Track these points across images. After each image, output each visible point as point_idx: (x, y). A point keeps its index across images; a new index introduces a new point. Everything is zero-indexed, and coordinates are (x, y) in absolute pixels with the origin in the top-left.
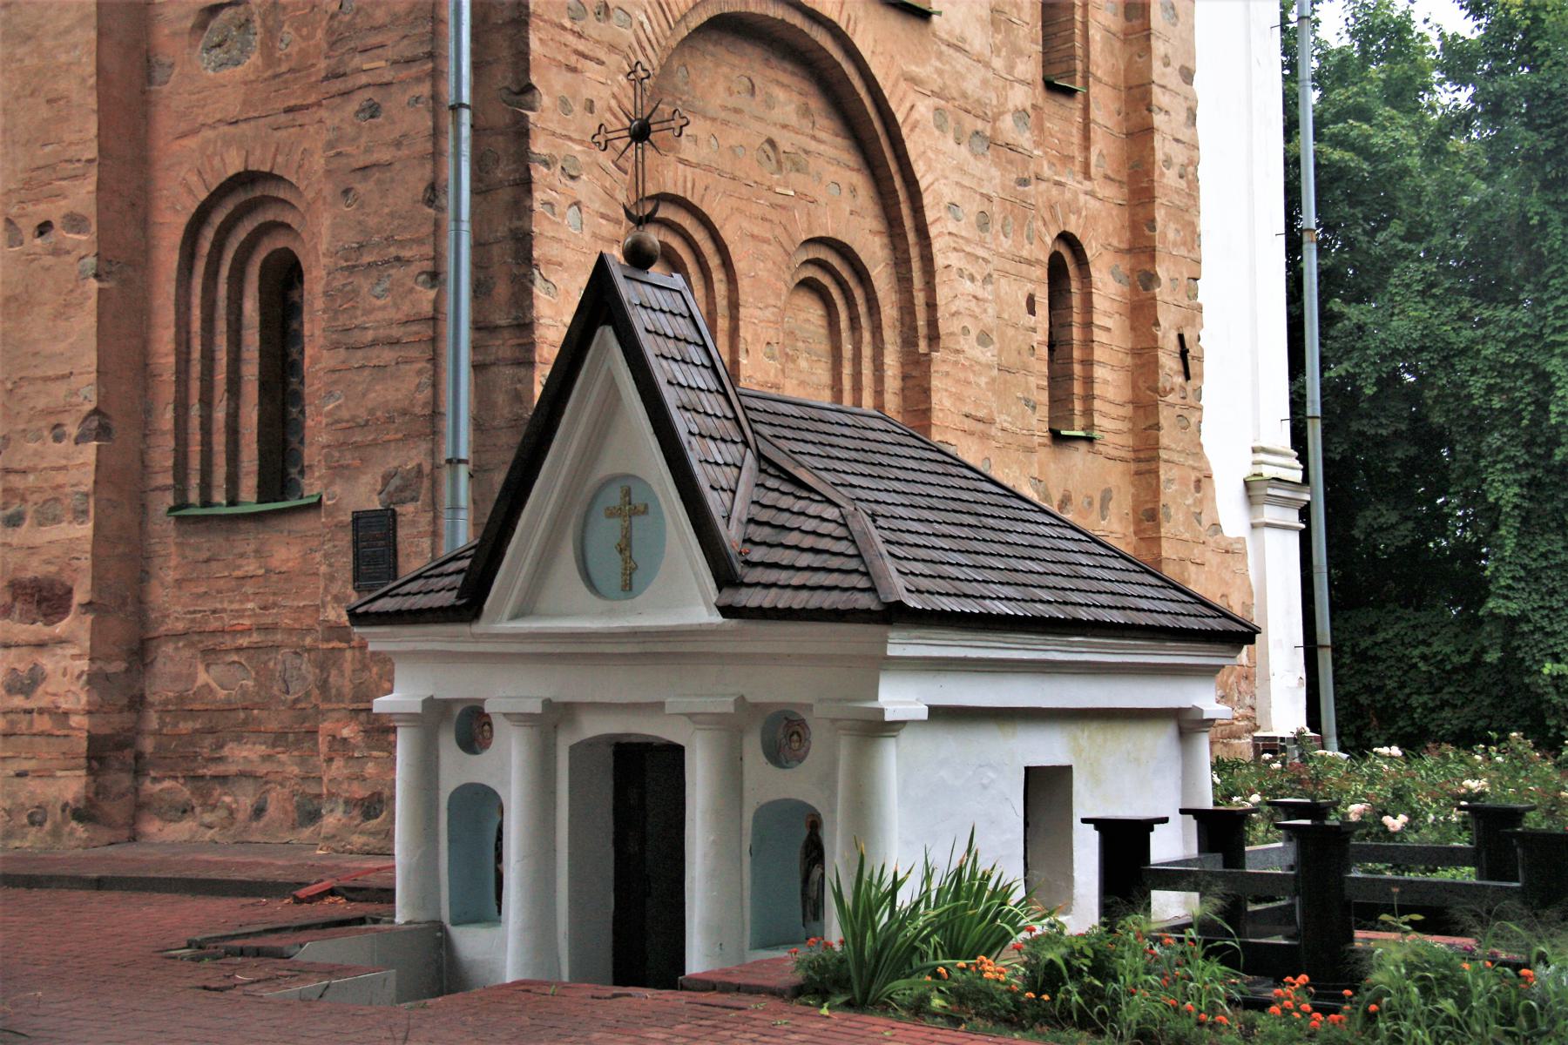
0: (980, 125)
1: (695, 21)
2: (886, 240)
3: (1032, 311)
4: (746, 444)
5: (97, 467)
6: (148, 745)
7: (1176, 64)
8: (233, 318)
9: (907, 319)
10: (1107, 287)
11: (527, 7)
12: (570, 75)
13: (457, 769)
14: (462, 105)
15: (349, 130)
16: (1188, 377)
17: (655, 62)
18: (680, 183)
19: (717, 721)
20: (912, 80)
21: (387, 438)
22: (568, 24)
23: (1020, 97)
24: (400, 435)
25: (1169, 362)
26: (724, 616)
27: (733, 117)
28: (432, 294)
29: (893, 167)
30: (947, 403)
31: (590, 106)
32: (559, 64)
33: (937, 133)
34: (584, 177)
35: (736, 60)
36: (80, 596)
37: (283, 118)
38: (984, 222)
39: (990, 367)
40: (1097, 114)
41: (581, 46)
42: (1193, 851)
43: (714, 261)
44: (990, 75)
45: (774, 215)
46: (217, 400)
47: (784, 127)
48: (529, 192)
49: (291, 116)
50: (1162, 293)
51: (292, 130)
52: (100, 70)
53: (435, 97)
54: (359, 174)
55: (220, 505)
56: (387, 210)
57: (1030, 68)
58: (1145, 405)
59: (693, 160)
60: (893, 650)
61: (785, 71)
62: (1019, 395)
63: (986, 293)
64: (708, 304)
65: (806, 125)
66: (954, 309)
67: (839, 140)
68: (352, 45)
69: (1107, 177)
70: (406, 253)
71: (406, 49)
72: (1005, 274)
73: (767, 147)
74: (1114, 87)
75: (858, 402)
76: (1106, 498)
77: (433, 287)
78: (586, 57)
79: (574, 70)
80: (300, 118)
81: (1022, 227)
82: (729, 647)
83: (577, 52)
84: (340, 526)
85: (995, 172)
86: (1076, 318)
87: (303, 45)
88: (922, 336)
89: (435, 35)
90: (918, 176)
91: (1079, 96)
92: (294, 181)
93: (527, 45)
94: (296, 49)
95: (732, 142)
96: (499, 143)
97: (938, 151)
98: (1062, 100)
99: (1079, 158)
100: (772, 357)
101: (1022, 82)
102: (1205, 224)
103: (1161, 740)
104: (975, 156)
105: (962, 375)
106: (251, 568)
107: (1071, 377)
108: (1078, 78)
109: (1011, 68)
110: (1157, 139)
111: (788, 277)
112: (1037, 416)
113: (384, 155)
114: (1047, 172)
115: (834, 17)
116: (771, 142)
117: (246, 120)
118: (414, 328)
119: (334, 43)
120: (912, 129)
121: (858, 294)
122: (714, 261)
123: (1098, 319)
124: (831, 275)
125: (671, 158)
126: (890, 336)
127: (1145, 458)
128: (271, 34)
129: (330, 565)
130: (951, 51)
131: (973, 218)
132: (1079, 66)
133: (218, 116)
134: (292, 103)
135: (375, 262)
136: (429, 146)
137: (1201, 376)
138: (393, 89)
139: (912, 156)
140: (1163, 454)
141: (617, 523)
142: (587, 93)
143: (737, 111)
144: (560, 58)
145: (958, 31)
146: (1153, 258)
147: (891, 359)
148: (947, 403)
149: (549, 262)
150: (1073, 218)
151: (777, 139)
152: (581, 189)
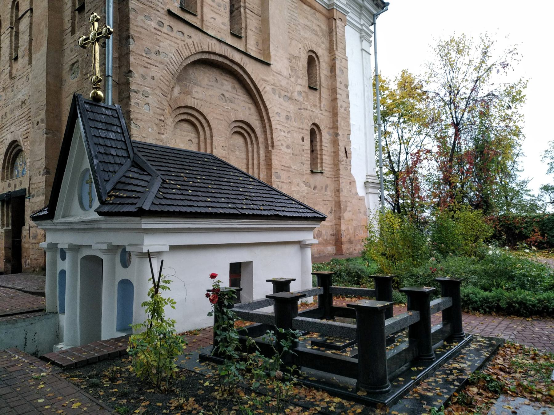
0: (286, 94)
1: (192, 59)
2: (260, 122)
4: (129, 157)
7: (343, 84)
10: (326, 136)
12: (145, 69)
14: (109, 76)
18: (193, 103)
20: (265, 81)
22: (145, 55)
23: (299, 88)
25: (342, 154)
27: (210, 87)
29: (260, 103)
30: (277, 162)
31: (153, 78)
32: (141, 66)
33: (273, 95)
34: (150, 97)
35: (211, 73)
38: (288, 118)
39: (290, 154)
40: (322, 95)
41: (149, 61)
42: (273, 293)
43: (205, 125)
44: (290, 82)
45: (223, 113)
48: (130, 100)
57: (304, 81)
58: (336, 165)
59: (197, 98)
60: (144, 226)
63: (289, 135)
65: (234, 91)
66: (278, 139)
67: (245, 96)
69: (326, 110)
72: (296, 131)
73: (222, 96)
74: (328, 89)
75: (206, 151)
76: (326, 187)
78: (151, 64)
82: (104, 226)
83: (147, 63)
86: (318, 144)
88: (270, 145)
91: (243, 39)
95: (210, 94)
97: (273, 99)
98: (314, 91)
99: (318, 105)
100: (224, 150)
101: (300, 85)
102: (352, 122)
103: (293, 250)
109: (296, 81)
111: (230, 130)
114: (309, 108)
115: (239, 62)
120: (265, 92)
121: (252, 135)
122: (205, 125)
123: (324, 144)
124: (243, 130)
125: (189, 96)
126: (262, 146)
127: (337, 177)
131: (284, 117)
132: (318, 83)
139: (265, 100)
140: (341, 176)
141: (88, 185)
142: (152, 74)
143: (211, 86)
144: (141, 64)
145: (279, 70)
147: (262, 152)
148: (277, 162)
149: (137, 119)
151: (225, 94)
152: (150, 100)
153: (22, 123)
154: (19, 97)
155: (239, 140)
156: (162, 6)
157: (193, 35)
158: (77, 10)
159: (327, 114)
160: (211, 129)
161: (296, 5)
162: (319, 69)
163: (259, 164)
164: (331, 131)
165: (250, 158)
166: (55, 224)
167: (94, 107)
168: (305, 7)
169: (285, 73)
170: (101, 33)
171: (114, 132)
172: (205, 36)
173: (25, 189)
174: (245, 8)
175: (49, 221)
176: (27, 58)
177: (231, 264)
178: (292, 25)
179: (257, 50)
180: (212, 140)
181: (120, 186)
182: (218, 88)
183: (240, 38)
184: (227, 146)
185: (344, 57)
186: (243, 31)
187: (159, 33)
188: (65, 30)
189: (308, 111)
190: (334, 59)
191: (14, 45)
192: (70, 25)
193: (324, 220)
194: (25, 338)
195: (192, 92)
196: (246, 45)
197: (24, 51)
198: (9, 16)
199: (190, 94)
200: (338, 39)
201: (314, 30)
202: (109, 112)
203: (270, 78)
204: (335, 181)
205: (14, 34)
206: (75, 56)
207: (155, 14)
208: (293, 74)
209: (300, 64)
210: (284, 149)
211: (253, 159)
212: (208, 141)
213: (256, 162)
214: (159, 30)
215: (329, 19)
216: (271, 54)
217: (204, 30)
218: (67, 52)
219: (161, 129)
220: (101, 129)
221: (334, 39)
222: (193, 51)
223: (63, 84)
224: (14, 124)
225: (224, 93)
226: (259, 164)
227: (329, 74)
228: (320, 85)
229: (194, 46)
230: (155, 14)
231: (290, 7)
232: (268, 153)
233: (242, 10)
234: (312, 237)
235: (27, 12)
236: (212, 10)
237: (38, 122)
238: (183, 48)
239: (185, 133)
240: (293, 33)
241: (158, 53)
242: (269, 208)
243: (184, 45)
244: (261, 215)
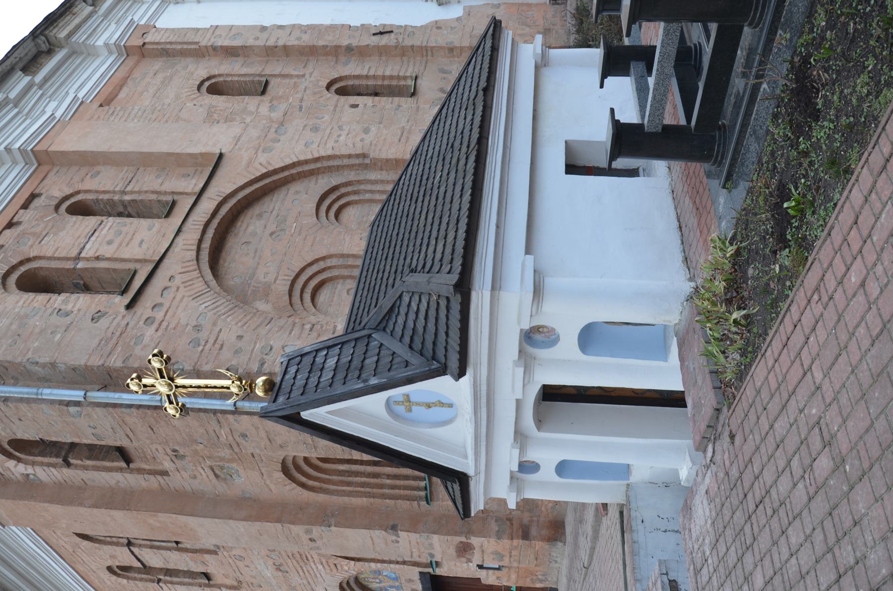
0: (273, 130)
1: (209, 276)
2: (320, 177)
3: (356, 106)
4: (369, 336)
5: (409, 531)
6: (539, 38)
7: (258, 34)
10: (352, 68)
12: (224, 348)
13: (547, 472)
16: (392, 32)
18: (284, 282)
19: (528, 370)
20: (249, 163)
22: (201, 348)
23: (264, 110)
25: (384, 40)
26: (464, 374)
29: (286, 173)
31: (240, 337)
32: (218, 354)
34: (271, 343)
36: (463, 539)
38: (315, 129)
40: (277, 72)
41: (211, 341)
47: (265, 227)
50: (355, 43)
52: (244, 520)
57: (251, 102)
58: (403, 52)
63: (346, 128)
65: (265, 215)
67: (276, 196)
69: (304, 67)
71: (214, 423)
73: (274, 236)
74: (267, 62)
76: (443, 71)
79: (222, 345)
83: (214, 345)
91: (176, 197)
98: (270, 88)
99: (296, 80)
101: (258, 108)
102: (327, 22)
103: (550, 79)
108: (261, 79)
109: (251, 113)
110: (289, 43)
111: (332, 227)
112: (403, 104)
113: (263, 434)
114: (299, 95)
115: (216, 203)
116: (272, 234)
120: (270, 164)
121: (343, 190)
123: (365, 73)
124: (332, 204)
125: (273, 287)
127: (425, 52)
128: (222, 459)
131: (313, 134)
132: (257, 79)
137: (392, 25)
140: (424, 44)
141: (414, 408)
142: (233, 338)
143: (256, 252)
146: (340, 47)
150: (320, 83)
153: (311, 572)
154: (269, 575)
156: (120, 317)
157: (169, 274)
158: (128, 465)
159: (310, 66)
160: (330, 256)
161: (119, 108)
162: (232, 75)
164: (342, 59)
166: (477, 473)
167: (282, 391)
168: (122, 95)
170: (160, 370)
171: (326, 360)
172: (169, 253)
173: (420, 573)
174: (124, 192)
175: (472, 484)
176: (207, 557)
177: (567, 173)
178: (154, 116)
181: (417, 345)
182: (260, 241)
183: (174, 203)
185: (211, 31)
186: (164, 198)
187: (165, 324)
188: (162, 489)
189: (305, 98)
190: (215, 48)
191: (187, 580)
192: (152, 477)
193: (500, 22)
194: (665, 531)
195: (266, 283)
197: (196, 562)
198: (140, 584)
200: (179, 40)
201: (162, 83)
202: (292, 370)
204: (432, 56)
205: (168, 578)
206: (202, 471)
207: (133, 329)
208: (238, 118)
210: (368, 138)
214: (160, 324)
215: (143, 56)
216: (204, 151)
217: (158, 258)
218: (196, 485)
219: (327, 330)
220: (319, 378)
221: (179, 47)
222: (196, 274)
223: (247, 495)
224: (314, 586)
225: (268, 232)
227: (240, 60)
228: (260, 75)
230: (133, 329)
231: (124, 118)
232: (375, 164)
233: (127, 198)
234: (530, 47)
235: (133, 553)
236: (128, 244)
237: (311, 540)
239: (335, 299)
240: (167, 116)
241: (198, 328)
242: (471, 107)
243: (185, 287)
244: (483, 116)
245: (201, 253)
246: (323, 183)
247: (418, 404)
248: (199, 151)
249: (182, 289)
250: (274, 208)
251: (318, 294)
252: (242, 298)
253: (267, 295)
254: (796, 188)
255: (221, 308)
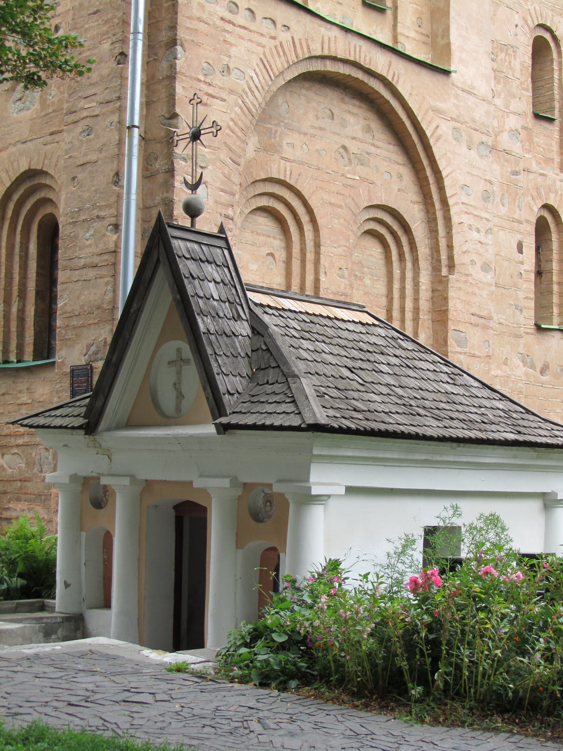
0: (484, 138)
1: (289, 76)
2: (422, 207)
3: (520, 251)
8: (23, 254)
9: (435, 254)
11: (175, 69)
15: (77, 143)
17: (260, 100)
18: (282, 172)
20: (437, 111)
21: (90, 322)
22: (202, 78)
23: (512, 122)
24: (96, 321)
28: (115, 237)
29: (425, 162)
33: (454, 142)
37: (49, 138)
38: (487, 196)
39: (490, 285)
41: (210, 90)
43: (305, 218)
46: (13, 302)
47: (353, 138)
48: (173, 176)
49: (53, 137)
51: (53, 145)
53: (121, 122)
54: (80, 168)
55: (12, 362)
56: (93, 189)
57: (523, 103)
60: (316, 452)
61: (354, 105)
62: (511, 302)
63: (489, 240)
64: (301, 244)
65: (368, 138)
66: (465, 249)
68: (80, 95)
70: (102, 214)
72: (503, 228)
73: (341, 150)
77: (116, 232)
78: (213, 97)
80: (56, 137)
81: (514, 200)
84: (65, 374)
85: (496, 167)
87: (61, 97)
88: (444, 265)
89: (122, 86)
90: (441, 169)
91: (389, 13)
92: (53, 174)
93: (174, 90)
94: (57, 99)
95: (318, 147)
96: (158, 148)
98: (545, 124)
100: (342, 277)
101: (514, 113)
104: (481, 157)
105: (470, 290)
106: (25, 399)
107: (551, 292)
111: (355, 229)
113: (93, 157)
114: (534, 167)
115: (385, 74)
116: (345, 148)
117: (31, 140)
118: (105, 257)
119: (71, 94)
120: (437, 141)
122: (305, 218)
124: (387, 229)
125: (276, 157)
126: (424, 265)
129: (59, 398)
130: (465, 94)
133: (17, 139)
134: (54, 129)
135: (86, 219)
136: (116, 150)
138: (99, 118)
141: (174, 369)
143: (321, 129)
145: (469, 82)
147: (425, 279)
148: (459, 306)
150: (552, 195)
155: (374, 250)
157: (292, 24)
163: (416, 310)
165: (396, 295)
169: (483, 87)
179: (418, 37)
180: (317, 253)
182: (335, 133)
184: (349, 267)
187: (230, 27)
189: (532, 176)
195: (281, 146)
196: (395, 26)
199: (276, 151)
203: (448, 105)
208: (500, 87)
209: (516, 64)
211: (403, 297)
212: (310, 256)
213: (409, 304)
214: (230, 22)
216: (453, 47)
226: (416, 310)
229: (295, 47)
238: (272, 53)
239: (261, 238)
243: (276, 47)
245: (319, 61)
246: (414, 214)
247: (179, 373)
248: (452, 40)
249: (273, 43)
250: (377, 147)
251: (265, 215)
252: (265, 119)
253: (265, 150)
254: (421, 650)
255: (251, 97)
